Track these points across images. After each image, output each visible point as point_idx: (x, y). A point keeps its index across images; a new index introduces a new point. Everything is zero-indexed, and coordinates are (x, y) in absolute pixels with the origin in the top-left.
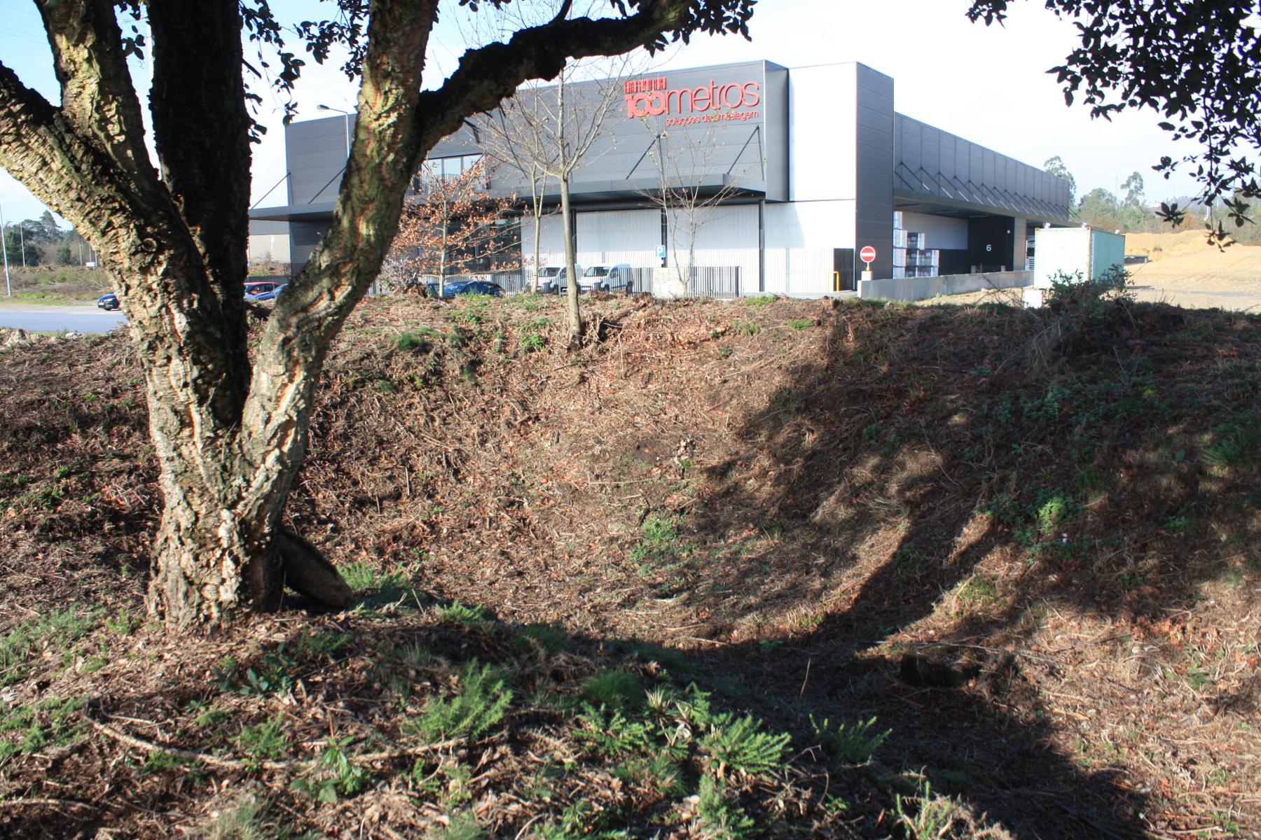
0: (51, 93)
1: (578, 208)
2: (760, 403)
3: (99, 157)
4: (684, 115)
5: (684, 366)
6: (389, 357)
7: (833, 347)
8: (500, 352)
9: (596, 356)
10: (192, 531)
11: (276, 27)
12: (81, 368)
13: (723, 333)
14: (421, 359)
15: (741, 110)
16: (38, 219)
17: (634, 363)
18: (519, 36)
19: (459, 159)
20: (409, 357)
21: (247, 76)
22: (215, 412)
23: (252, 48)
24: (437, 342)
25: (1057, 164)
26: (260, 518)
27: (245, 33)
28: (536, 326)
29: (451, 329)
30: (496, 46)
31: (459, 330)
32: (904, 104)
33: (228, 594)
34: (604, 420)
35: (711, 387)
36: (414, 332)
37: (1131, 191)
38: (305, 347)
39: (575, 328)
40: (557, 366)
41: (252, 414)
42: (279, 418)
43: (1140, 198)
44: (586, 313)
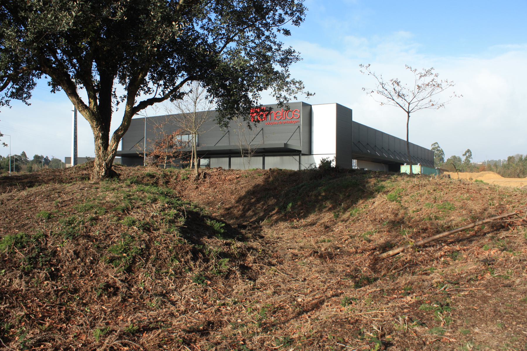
0: (88, 105)
1: (232, 155)
2: (243, 193)
3: (93, 113)
4: (272, 121)
5: (226, 186)
6: (143, 178)
7: (266, 180)
8: (175, 180)
9: (202, 182)
10: (99, 165)
11: (116, 97)
12: (63, 173)
13: (239, 177)
14: (152, 179)
15: (292, 120)
16: (20, 155)
17: (212, 184)
18: (148, 100)
19: (188, 136)
20: (149, 178)
21: (112, 104)
22: (104, 148)
23: (113, 99)
24: (157, 176)
25: (437, 145)
26: (109, 163)
27: (112, 97)
28: (186, 174)
29: (162, 173)
30: (145, 101)
31: (164, 174)
32: (356, 118)
33: (103, 174)
34: (201, 197)
35: (232, 190)
36: (151, 173)
37: (467, 157)
38: (117, 139)
39: (197, 174)
40: (191, 184)
41: (109, 149)
42: (113, 149)
43: (470, 160)
44: (200, 171)
